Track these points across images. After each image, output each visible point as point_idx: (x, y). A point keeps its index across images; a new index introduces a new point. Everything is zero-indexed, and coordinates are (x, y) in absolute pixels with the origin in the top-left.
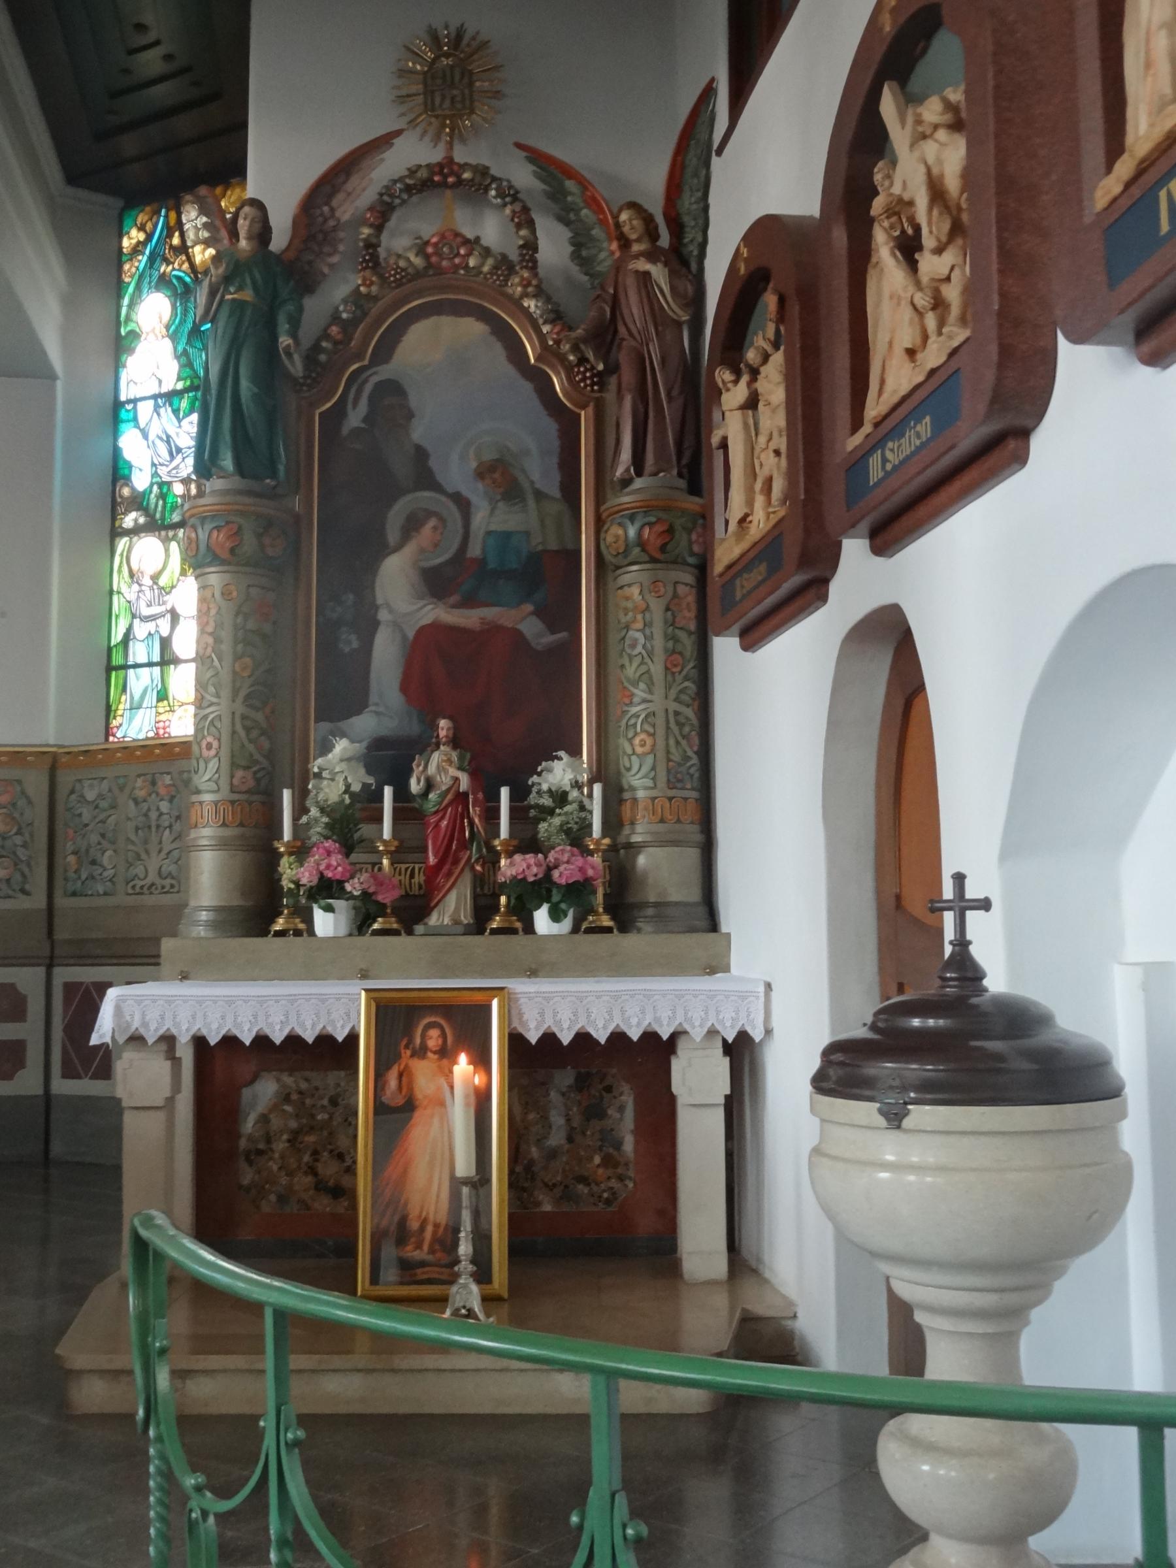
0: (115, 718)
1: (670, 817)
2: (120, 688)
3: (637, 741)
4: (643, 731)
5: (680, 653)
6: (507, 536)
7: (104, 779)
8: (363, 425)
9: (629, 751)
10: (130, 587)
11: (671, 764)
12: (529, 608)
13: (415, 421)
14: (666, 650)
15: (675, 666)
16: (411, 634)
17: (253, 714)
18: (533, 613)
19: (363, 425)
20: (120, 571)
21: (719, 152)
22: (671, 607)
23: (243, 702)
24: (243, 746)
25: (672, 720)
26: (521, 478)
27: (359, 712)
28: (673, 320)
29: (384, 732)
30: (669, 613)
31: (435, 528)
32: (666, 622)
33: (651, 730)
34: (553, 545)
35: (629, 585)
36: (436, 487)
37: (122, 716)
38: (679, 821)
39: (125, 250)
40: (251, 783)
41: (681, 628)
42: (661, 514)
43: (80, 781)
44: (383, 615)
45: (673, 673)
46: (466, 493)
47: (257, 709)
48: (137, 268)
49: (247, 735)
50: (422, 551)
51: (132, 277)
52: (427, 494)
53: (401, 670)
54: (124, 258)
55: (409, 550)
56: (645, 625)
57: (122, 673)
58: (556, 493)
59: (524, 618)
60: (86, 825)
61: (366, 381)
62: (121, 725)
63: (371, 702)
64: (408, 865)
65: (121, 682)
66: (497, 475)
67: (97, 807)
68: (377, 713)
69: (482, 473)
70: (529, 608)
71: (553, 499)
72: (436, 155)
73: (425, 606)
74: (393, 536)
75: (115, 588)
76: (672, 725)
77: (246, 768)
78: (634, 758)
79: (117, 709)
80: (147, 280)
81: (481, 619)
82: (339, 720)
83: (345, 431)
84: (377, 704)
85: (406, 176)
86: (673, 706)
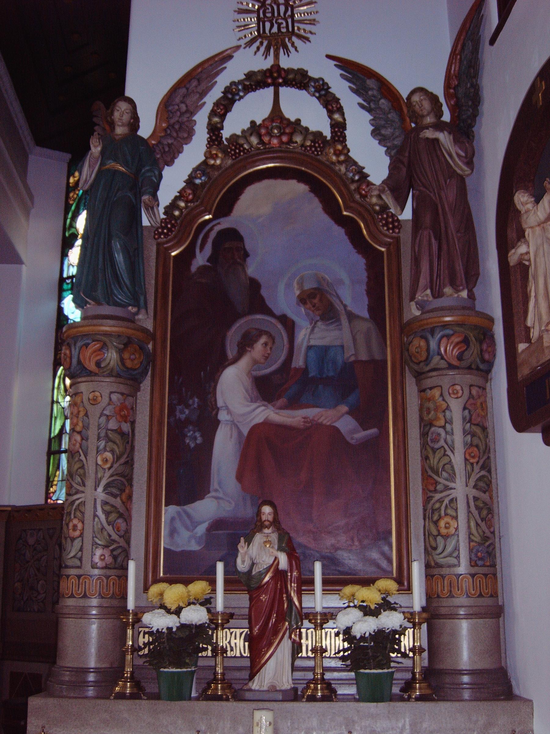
0: (52, 487)
1: (473, 592)
2: (56, 466)
3: (442, 524)
4: (446, 514)
5: (477, 446)
6: (325, 349)
7: (40, 530)
8: (208, 264)
9: (435, 532)
10: (64, 398)
11: (472, 544)
12: (344, 408)
13: (249, 260)
14: (465, 444)
15: (473, 457)
16: (245, 432)
17: (111, 500)
18: (348, 413)
19: (208, 264)
20: (59, 388)
21: (492, 41)
22: (467, 406)
23: (104, 490)
24: (103, 528)
25: (472, 503)
26: (335, 300)
27: (202, 498)
28: (458, 175)
29: (223, 514)
30: (467, 412)
31: (266, 344)
32: (464, 419)
33: (454, 514)
34: (364, 356)
35: (431, 389)
36: (269, 312)
37: (56, 485)
38: (481, 595)
39: (71, 185)
40: (109, 559)
41: (477, 425)
42: (457, 329)
43: (25, 531)
44: (223, 416)
45: (472, 464)
46: (290, 314)
47: (115, 496)
48: (78, 195)
49: (107, 519)
50: (255, 362)
51: (74, 200)
52: (258, 316)
53: (237, 462)
54: (70, 189)
55: (244, 362)
56: (446, 422)
57: (57, 456)
58: (365, 314)
59: (339, 418)
60: (28, 562)
61: (211, 229)
62: (55, 491)
63: (211, 488)
64: (242, 630)
65: (56, 462)
66: (316, 301)
67: (35, 549)
68: (217, 498)
69: (303, 300)
70: (344, 408)
71: (363, 319)
72: (267, 64)
73: (259, 407)
74: (231, 353)
75: (55, 399)
76: (473, 508)
77: (106, 547)
78: (439, 539)
79: (53, 481)
80: (83, 201)
81: (304, 418)
82: (184, 505)
83: (194, 269)
84: (216, 490)
85: (244, 80)
86: (475, 492)
